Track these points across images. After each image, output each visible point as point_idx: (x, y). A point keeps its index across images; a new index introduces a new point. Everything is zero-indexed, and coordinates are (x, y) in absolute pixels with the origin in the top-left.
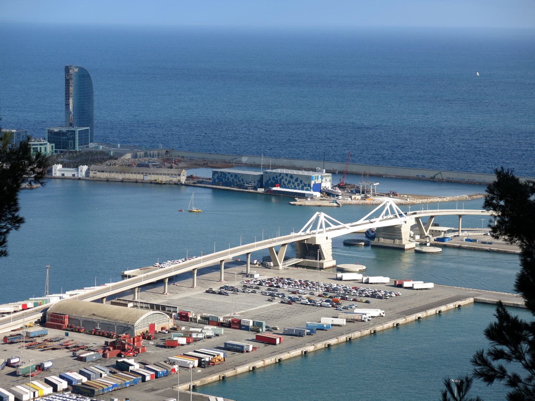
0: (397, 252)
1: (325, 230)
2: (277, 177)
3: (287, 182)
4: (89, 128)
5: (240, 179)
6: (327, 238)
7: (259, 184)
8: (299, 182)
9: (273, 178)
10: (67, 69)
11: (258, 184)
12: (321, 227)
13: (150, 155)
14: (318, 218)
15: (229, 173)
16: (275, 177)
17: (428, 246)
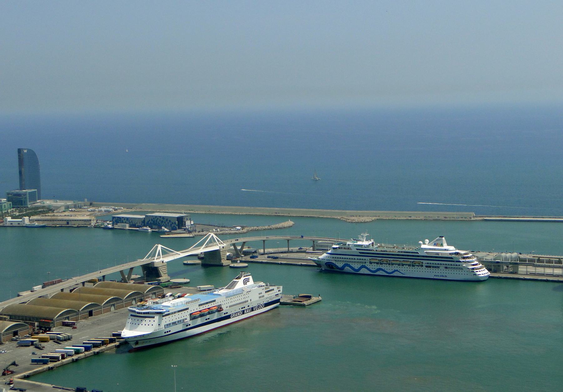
0: (219, 268)
1: (161, 257)
2: (154, 219)
3: (161, 222)
4: (36, 190)
5: (130, 221)
6: (163, 262)
7: (143, 224)
9: (152, 220)
10: (20, 151)
11: (142, 224)
12: (159, 255)
13: (78, 206)
14: (157, 247)
15: (123, 217)
16: (153, 219)
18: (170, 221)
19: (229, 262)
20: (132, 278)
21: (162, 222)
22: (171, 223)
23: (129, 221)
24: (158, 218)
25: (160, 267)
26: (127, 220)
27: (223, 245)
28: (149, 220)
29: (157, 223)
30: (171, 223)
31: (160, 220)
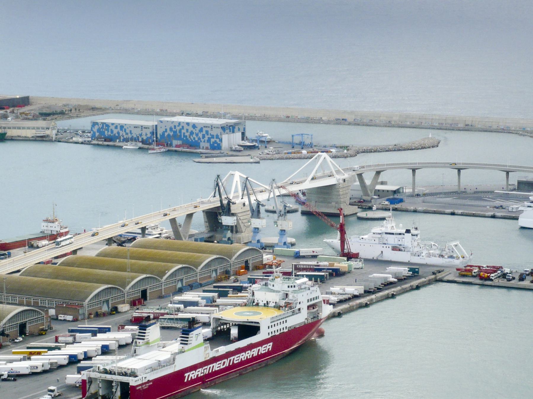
2: (175, 126)
5: (128, 131)
9: (171, 129)
16: (173, 127)
18: (207, 132)
19: (355, 209)
20: (190, 234)
21: (192, 133)
22: (210, 136)
23: (125, 131)
24: (183, 127)
25: (239, 213)
26: (121, 129)
27: (344, 177)
28: (164, 130)
29: (181, 135)
31: (187, 130)
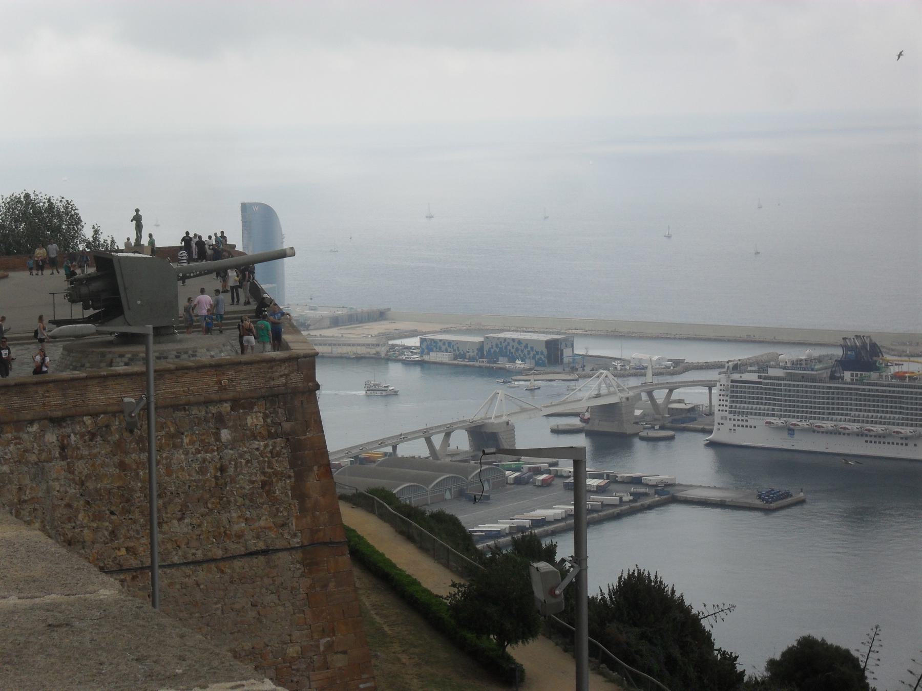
8: (529, 349)
17: (657, 430)
22: (534, 353)
30: (534, 353)
